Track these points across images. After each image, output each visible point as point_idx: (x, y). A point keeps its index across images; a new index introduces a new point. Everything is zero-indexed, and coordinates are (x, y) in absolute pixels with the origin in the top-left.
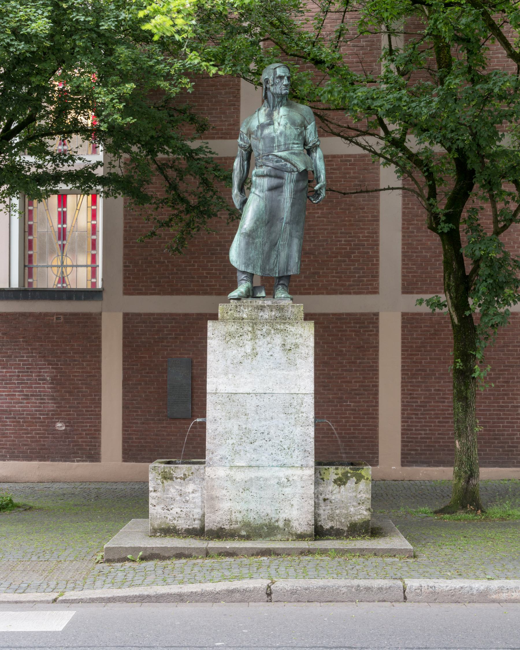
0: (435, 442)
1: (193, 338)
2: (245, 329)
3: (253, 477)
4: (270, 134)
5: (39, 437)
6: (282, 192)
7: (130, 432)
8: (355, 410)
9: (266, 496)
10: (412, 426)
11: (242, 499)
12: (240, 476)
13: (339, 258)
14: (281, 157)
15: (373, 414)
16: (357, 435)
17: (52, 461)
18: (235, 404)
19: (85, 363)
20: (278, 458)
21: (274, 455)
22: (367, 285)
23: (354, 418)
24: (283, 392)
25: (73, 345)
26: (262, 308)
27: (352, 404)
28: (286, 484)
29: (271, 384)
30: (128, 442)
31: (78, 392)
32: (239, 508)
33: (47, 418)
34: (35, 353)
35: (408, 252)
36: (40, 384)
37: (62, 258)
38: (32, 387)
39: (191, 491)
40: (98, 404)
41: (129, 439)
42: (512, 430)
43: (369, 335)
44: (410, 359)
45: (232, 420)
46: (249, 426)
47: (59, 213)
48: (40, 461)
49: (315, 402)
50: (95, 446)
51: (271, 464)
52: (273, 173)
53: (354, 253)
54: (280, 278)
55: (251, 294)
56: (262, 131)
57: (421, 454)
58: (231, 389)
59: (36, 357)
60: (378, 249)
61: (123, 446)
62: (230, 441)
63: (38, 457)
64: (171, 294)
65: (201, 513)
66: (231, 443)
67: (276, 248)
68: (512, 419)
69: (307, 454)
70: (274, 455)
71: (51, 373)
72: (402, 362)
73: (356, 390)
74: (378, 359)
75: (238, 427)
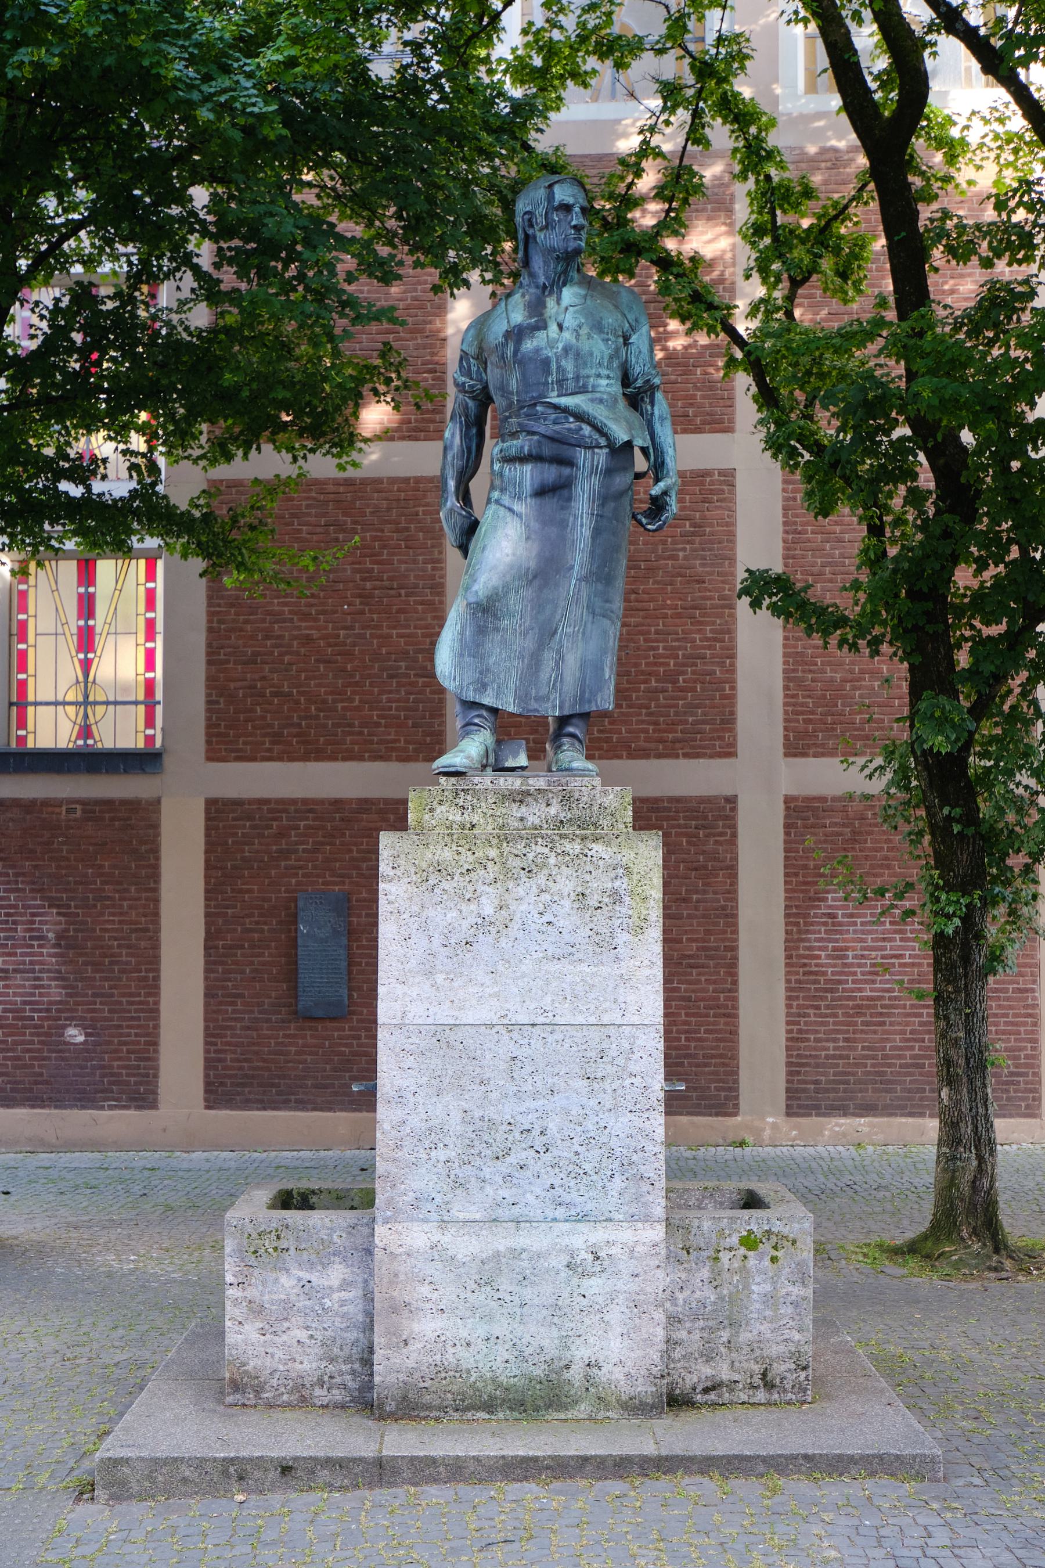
0: (856, 1065)
1: (351, 851)
2: (479, 854)
3: (502, 1248)
4: (537, 350)
5: (31, 1058)
6: (569, 499)
7: (219, 1047)
8: (689, 999)
9: (536, 1301)
10: (807, 1032)
11: (474, 1309)
12: (466, 1246)
13: (654, 684)
14: (566, 410)
15: (727, 1007)
16: (692, 1051)
17: (56, 1107)
18: (452, 1053)
19: (125, 903)
20: (566, 1198)
21: (559, 1191)
22: (712, 739)
23: (687, 1015)
24: (580, 1019)
25: (101, 867)
26: (521, 797)
27: (683, 986)
28: (590, 1269)
29: (548, 999)
30: (216, 1068)
31: (111, 963)
32: (464, 1334)
33: (48, 1018)
34: (23, 882)
35: (794, 671)
36: (32, 946)
37: (86, 687)
38: (15, 954)
39: (336, 1283)
40: (153, 987)
41: (220, 1060)
42: (1016, 1040)
43: (716, 842)
44: (802, 891)
45: (447, 1098)
46: (491, 1112)
47: (80, 596)
48: (33, 1107)
49: (667, 1048)
50: (147, 1075)
51: (550, 1215)
52: (547, 450)
53: (684, 673)
54: (563, 721)
55: (492, 760)
56: (519, 342)
57: (827, 1091)
58: (444, 1015)
59: (24, 890)
60: (733, 665)
61: (206, 1076)
62: (441, 1154)
63: (28, 1099)
64: (305, 758)
65: (364, 1341)
66: (442, 1159)
67: (554, 644)
68: (1016, 1015)
69: (645, 1187)
70: (559, 1191)
71: (56, 924)
72: (787, 899)
73: (690, 957)
74: (736, 891)
75: (461, 1114)
